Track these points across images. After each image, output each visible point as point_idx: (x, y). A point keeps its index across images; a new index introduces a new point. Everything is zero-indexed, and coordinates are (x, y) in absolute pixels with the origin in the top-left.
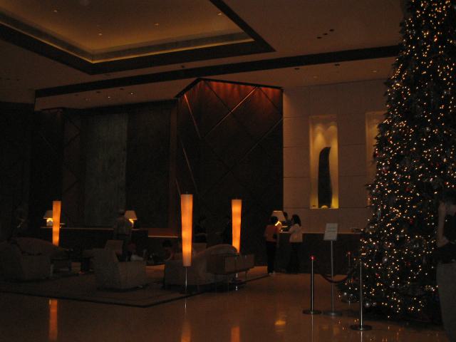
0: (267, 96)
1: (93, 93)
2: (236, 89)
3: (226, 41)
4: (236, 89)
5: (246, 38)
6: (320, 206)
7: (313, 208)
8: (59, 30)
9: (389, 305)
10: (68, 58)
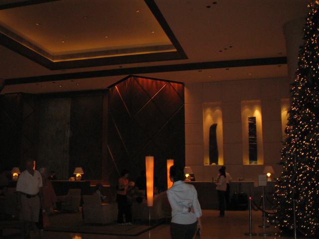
0: (174, 88)
1: (69, 81)
2: (154, 83)
3: (152, 51)
4: (154, 83)
5: (172, 49)
6: (211, 163)
7: (207, 165)
8: (34, 38)
9: (307, 227)
10: (38, 57)
